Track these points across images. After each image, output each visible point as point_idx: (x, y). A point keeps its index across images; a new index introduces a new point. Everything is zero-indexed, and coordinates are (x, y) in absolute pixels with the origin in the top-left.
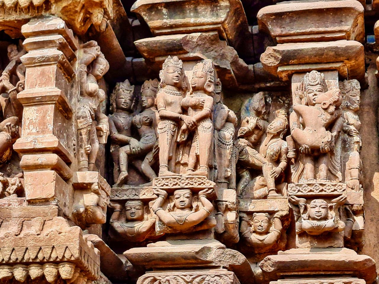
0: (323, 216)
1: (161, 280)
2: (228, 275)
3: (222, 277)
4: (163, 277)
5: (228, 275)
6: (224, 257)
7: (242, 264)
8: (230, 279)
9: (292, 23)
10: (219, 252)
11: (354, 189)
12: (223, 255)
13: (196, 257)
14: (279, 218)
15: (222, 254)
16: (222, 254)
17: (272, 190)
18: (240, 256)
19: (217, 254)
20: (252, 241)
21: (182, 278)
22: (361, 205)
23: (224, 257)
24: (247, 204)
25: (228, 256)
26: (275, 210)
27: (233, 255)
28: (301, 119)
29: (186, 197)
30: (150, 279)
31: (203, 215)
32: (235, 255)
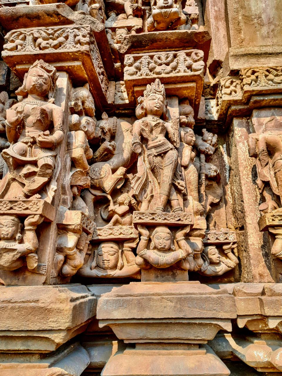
0: (169, 4)
1: (26, 34)
2: (86, 28)
3: (80, 29)
4: (28, 31)
5: (86, 28)
6: (85, 22)
7: (101, 31)
8: (87, 30)
9: (141, 113)
10: (81, 17)
11: (191, 6)
12: (84, 20)
13: (57, 12)
14: (135, 30)
15: (83, 19)
16: (83, 19)
17: (131, 15)
18: (99, 24)
19: (78, 18)
20: (114, 47)
21: (45, 32)
22: (196, 14)
23: (85, 22)
24: (111, 23)
25: (88, 22)
26: (132, 26)
27: (93, 22)
28: (139, 151)
29: (71, 22)
30: (16, 34)
31: (154, 328)
32: (95, 22)
